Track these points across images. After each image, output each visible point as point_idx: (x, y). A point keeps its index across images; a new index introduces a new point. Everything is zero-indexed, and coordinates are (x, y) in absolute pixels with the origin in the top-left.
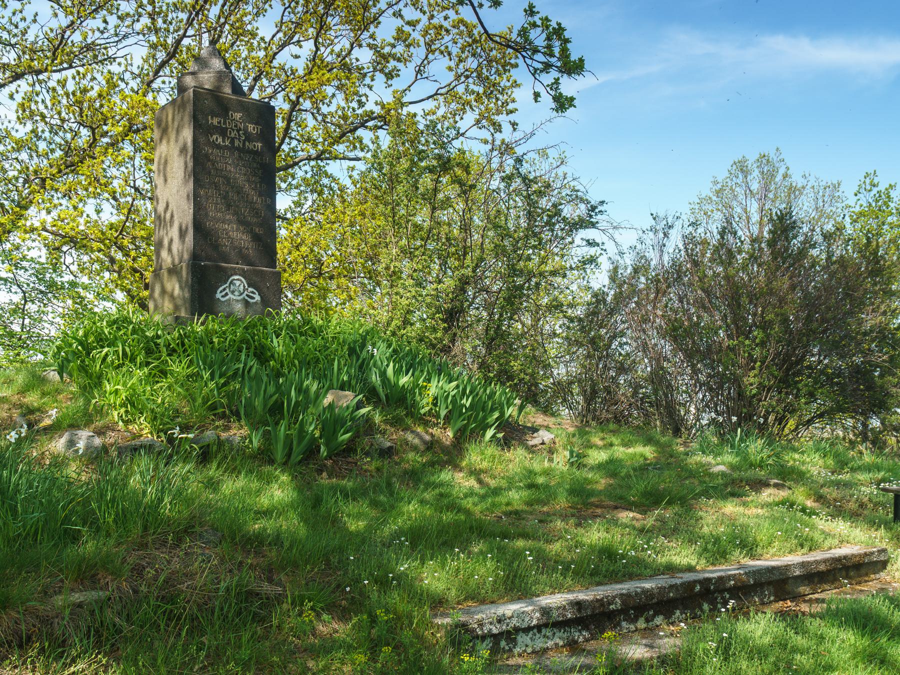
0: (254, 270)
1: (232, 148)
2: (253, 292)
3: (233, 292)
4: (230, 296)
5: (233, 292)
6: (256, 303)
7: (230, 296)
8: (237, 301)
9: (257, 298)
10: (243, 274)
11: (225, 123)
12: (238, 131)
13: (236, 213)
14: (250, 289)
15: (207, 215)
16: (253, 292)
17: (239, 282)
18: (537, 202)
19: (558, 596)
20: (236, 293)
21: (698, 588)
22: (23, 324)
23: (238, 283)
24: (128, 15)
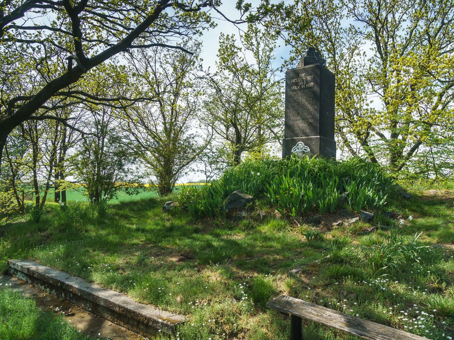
0: (308, 139)
1: (301, 89)
2: (307, 148)
3: (298, 149)
4: (297, 150)
5: (298, 149)
6: (308, 152)
7: (297, 150)
8: (300, 152)
9: (309, 150)
10: (303, 140)
11: (298, 80)
12: (303, 81)
13: (301, 116)
14: (306, 146)
15: (290, 119)
16: (307, 148)
17: (301, 144)
18: (123, 165)
19: (402, 334)
20: (300, 149)
21: (59, 284)
22: (348, 146)
23: (300, 145)
24: (296, 42)
